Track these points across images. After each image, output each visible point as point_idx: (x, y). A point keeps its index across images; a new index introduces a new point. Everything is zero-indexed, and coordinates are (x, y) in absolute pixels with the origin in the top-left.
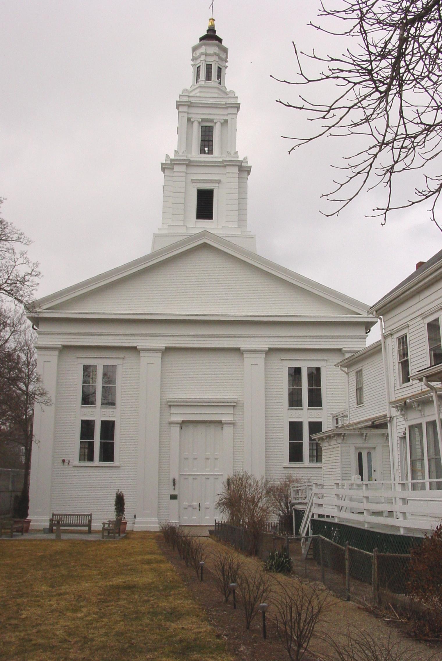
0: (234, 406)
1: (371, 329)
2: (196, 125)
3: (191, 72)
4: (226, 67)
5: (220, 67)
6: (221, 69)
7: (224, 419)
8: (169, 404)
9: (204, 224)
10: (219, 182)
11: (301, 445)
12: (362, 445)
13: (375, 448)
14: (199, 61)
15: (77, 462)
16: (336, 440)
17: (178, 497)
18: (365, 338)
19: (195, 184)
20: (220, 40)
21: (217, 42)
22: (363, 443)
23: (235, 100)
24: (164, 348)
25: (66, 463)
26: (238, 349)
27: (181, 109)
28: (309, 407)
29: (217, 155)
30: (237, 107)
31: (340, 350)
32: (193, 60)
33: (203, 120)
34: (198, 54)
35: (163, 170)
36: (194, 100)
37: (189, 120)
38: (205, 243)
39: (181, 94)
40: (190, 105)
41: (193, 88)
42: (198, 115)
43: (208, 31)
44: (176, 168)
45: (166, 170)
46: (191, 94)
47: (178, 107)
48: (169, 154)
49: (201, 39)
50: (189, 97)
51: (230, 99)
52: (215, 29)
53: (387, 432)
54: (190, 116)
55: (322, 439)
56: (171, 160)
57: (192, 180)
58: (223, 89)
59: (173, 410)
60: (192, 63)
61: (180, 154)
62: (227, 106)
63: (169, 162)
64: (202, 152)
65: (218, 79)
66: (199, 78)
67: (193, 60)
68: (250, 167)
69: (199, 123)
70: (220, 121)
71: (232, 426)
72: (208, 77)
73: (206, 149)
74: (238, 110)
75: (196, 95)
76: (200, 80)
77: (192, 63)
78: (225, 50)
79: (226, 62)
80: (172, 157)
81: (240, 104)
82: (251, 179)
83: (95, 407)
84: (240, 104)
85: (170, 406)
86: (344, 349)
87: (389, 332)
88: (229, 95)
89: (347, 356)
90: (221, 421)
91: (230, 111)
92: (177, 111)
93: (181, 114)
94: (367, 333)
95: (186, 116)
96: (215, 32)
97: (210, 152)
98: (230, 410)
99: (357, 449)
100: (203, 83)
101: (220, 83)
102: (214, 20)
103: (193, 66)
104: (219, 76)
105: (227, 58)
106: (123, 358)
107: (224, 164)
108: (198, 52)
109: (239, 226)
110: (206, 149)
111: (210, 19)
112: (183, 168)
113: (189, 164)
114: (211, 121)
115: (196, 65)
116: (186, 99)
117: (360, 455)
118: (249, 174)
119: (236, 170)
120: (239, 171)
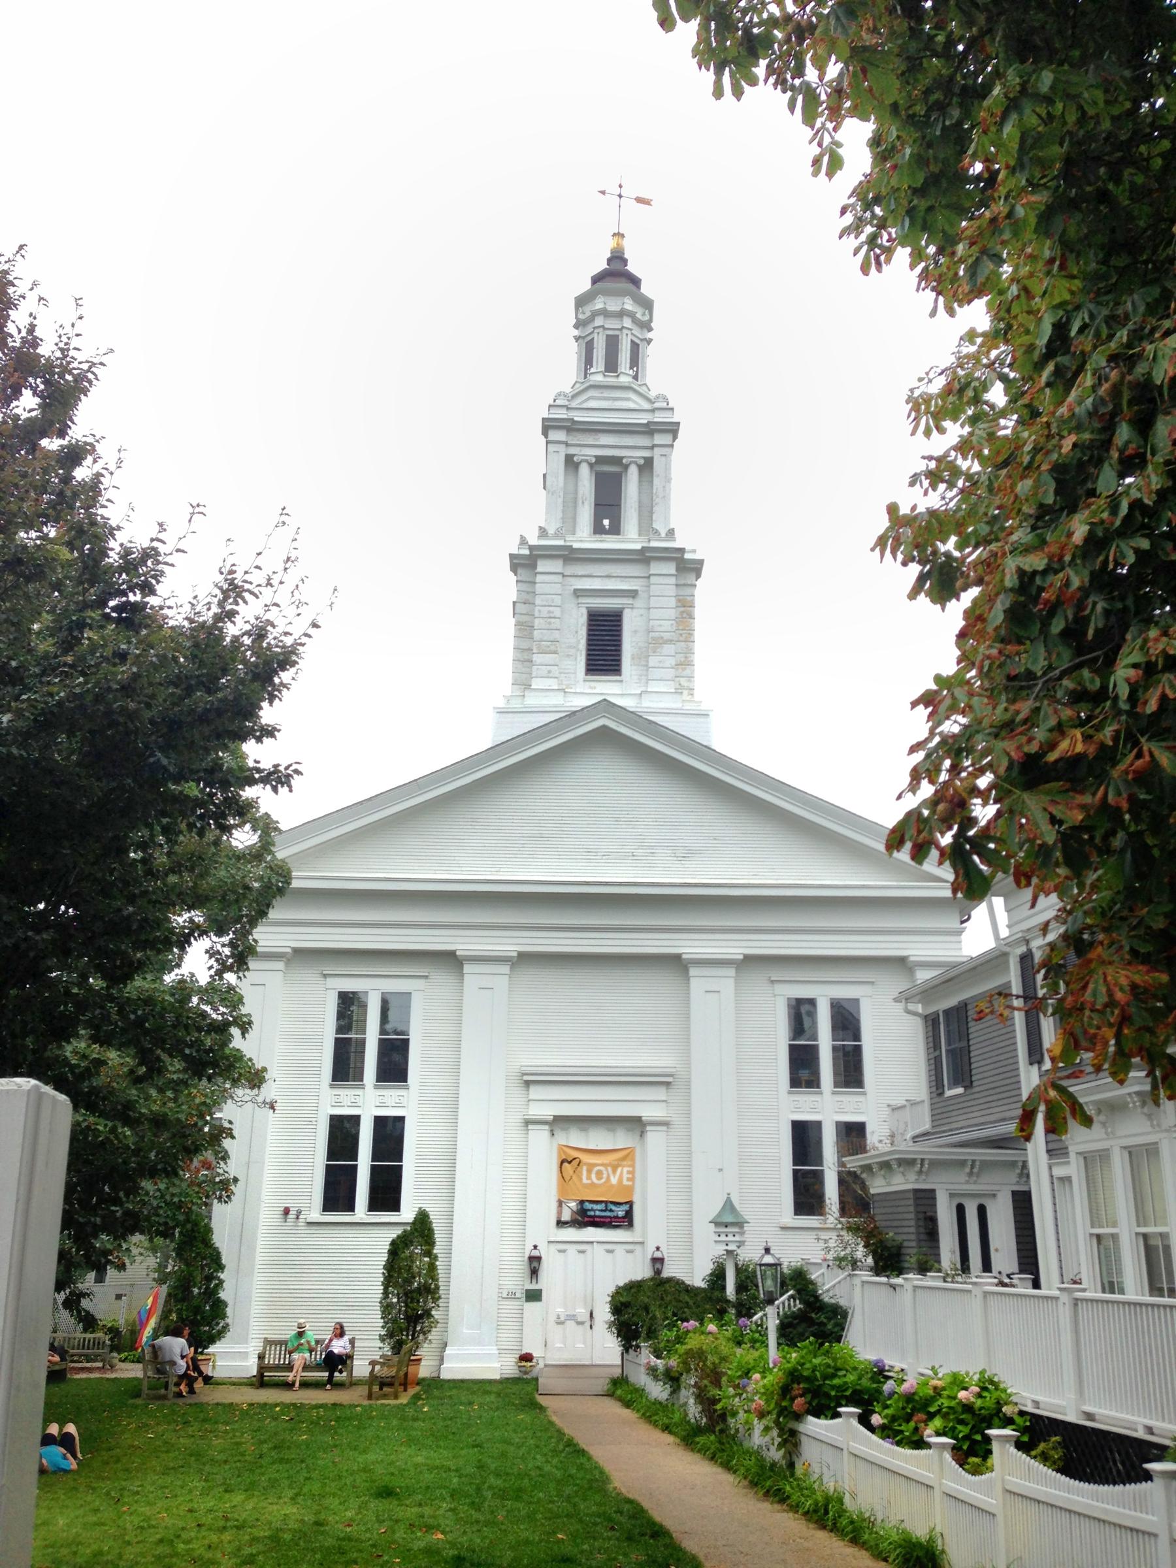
0: (668, 1084)
1: (973, 913)
2: (584, 470)
3: (571, 352)
4: (649, 341)
5: (637, 341)
6: (638, 345)
7: (647, 1112)
8: (526, 1078)
9: (605, 688)
10: (633, 594)
11: (818, 1177)
12: (965, 1187)
13: (994, 1195)
14: (589, 329)
15: (316, 1214)
16: (904, 1175)
17: (544, 1294)
18: (960, 932)
19: (581, 600)
20: (635, 281)
21: (630, 286)
22: (967, 1182)
23: (668, 414)
24: (515, 954)
25: (292, 1215)
26: (678, 957)
27: (555, 435)
28: (835, 1087)
29: (631, 539)
30: (673, 430)
31: (901, 961)
32: (576, 326)
33: (600, 460)
34: (588, 314)
35: (514, 568)
36: (579, 417)
37: (569, 459)
38: (604, 727)
39: (552, 403)
40: (571, 427)
41: (579, 387)
42: (590, 448)
43: (609, 261)
44: (542, 566)
45: (519, 571)
46: (574, 404)
47: (545, 431)
48: (947, 316)
49: (596, 280)
50: (568, 409)
51: (657, 414)
52: (626, 256)
53: (1023, 1159)
54: (572, 451)
55: (868, 1168)
56: (531, 548)
57: (576, 591)
58: (643, 390)
59: (536, 1092)
60: (576, 333)
61: (551, 531)
62: (649, 430)
63: (527, 552)
64: (598, 529)
65: (631, 368)
66: (591, 366)
67: (576, 326)
68: (701, 562)
69: (591, 465)
70: (635, 463)
71: (664, 1128)
72: (611, 366)
73: (606, 522)
74: (675, 438)
75: (585, 405)
76: (593, 370)
77: (576, 333)
78: (647, 304)
79: (650, 329)
80: (533, 540)
81: (678, 424)
82: (704, 590)
83: (363, 1087)
84: (678, 424)
85: (528, 1084)
86: (912, 959)
87: (1020, 935)
88: (657, 405)
89: (923, 976)
90: (640, 1117)
91: (659, 439)
92: (544, 440)
93: (552, 448)
94: (963, 922)
95: (563, 451)
96: (625, 262)
97: (615, 529)
98: (660, 1093)
99: (952, 1195)
100: (599, 378)
101: (636, 378)
102: (623, 236)
103: (577, 339)
104: (635, 361)
105: (651, 320)
106: (426, 977)
107: (644, 557)
108: (588, 310)
109: (678, 692)
110: (606, 522)
111: (614, 235)
112: (556, 566)
113: (570, 556)
114: (617, 461)
115: (584, 338)
116: (561, 414)
117: (961, 1210)
118: (698, 576)
119: (671, 568)
120: (677, 570)
